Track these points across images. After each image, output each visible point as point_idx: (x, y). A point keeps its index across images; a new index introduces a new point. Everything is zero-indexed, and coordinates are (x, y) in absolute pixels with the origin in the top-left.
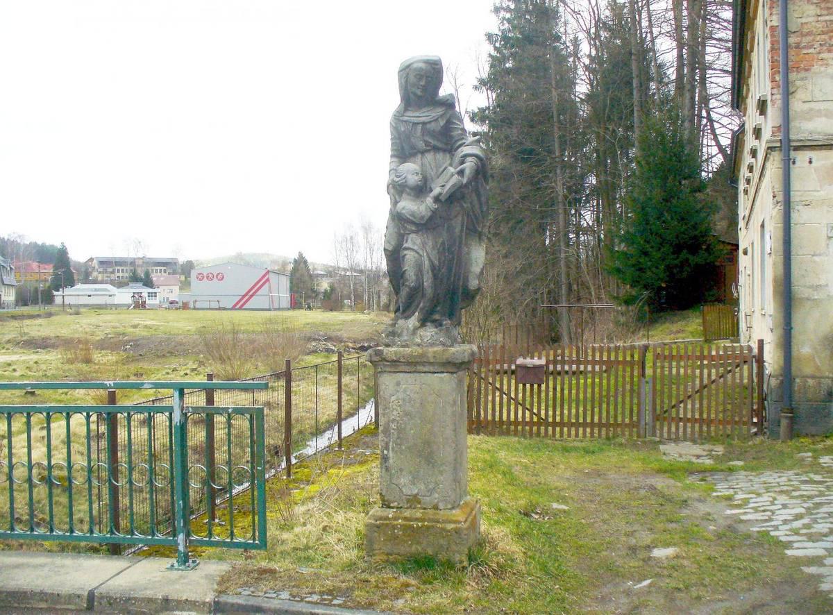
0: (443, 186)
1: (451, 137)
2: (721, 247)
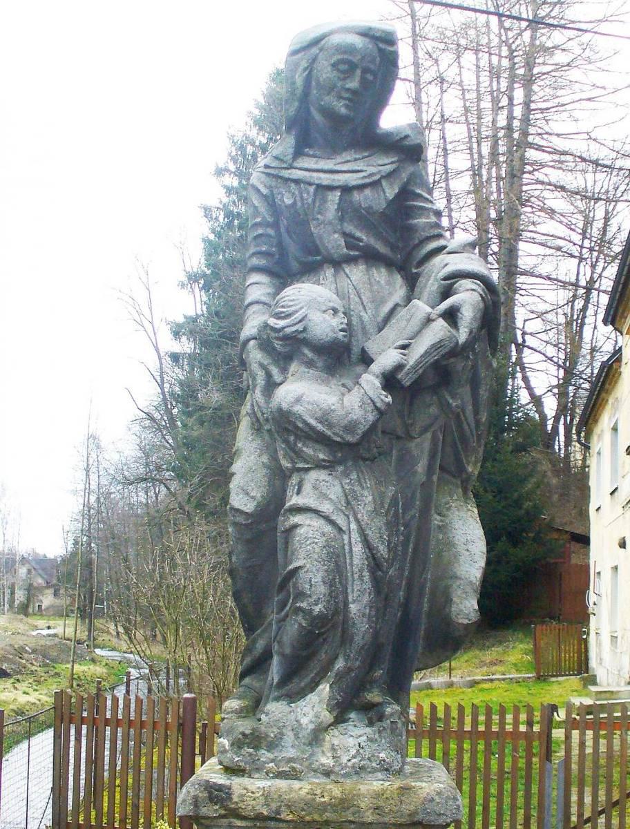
0: (404, 347)
1: (411, 229)
2: (555, 535)
